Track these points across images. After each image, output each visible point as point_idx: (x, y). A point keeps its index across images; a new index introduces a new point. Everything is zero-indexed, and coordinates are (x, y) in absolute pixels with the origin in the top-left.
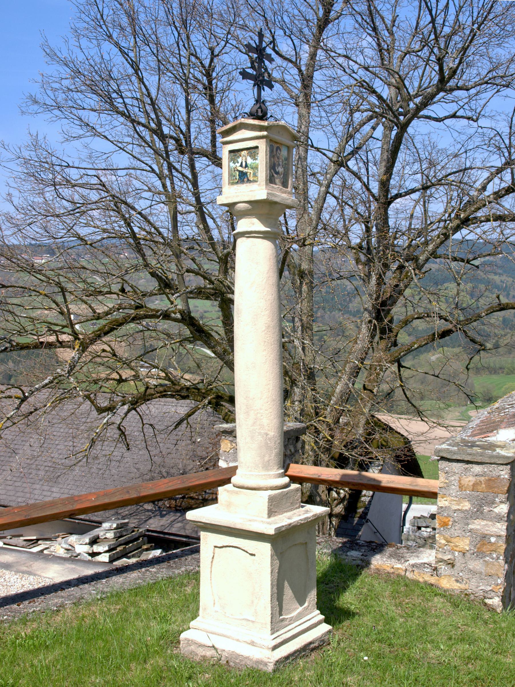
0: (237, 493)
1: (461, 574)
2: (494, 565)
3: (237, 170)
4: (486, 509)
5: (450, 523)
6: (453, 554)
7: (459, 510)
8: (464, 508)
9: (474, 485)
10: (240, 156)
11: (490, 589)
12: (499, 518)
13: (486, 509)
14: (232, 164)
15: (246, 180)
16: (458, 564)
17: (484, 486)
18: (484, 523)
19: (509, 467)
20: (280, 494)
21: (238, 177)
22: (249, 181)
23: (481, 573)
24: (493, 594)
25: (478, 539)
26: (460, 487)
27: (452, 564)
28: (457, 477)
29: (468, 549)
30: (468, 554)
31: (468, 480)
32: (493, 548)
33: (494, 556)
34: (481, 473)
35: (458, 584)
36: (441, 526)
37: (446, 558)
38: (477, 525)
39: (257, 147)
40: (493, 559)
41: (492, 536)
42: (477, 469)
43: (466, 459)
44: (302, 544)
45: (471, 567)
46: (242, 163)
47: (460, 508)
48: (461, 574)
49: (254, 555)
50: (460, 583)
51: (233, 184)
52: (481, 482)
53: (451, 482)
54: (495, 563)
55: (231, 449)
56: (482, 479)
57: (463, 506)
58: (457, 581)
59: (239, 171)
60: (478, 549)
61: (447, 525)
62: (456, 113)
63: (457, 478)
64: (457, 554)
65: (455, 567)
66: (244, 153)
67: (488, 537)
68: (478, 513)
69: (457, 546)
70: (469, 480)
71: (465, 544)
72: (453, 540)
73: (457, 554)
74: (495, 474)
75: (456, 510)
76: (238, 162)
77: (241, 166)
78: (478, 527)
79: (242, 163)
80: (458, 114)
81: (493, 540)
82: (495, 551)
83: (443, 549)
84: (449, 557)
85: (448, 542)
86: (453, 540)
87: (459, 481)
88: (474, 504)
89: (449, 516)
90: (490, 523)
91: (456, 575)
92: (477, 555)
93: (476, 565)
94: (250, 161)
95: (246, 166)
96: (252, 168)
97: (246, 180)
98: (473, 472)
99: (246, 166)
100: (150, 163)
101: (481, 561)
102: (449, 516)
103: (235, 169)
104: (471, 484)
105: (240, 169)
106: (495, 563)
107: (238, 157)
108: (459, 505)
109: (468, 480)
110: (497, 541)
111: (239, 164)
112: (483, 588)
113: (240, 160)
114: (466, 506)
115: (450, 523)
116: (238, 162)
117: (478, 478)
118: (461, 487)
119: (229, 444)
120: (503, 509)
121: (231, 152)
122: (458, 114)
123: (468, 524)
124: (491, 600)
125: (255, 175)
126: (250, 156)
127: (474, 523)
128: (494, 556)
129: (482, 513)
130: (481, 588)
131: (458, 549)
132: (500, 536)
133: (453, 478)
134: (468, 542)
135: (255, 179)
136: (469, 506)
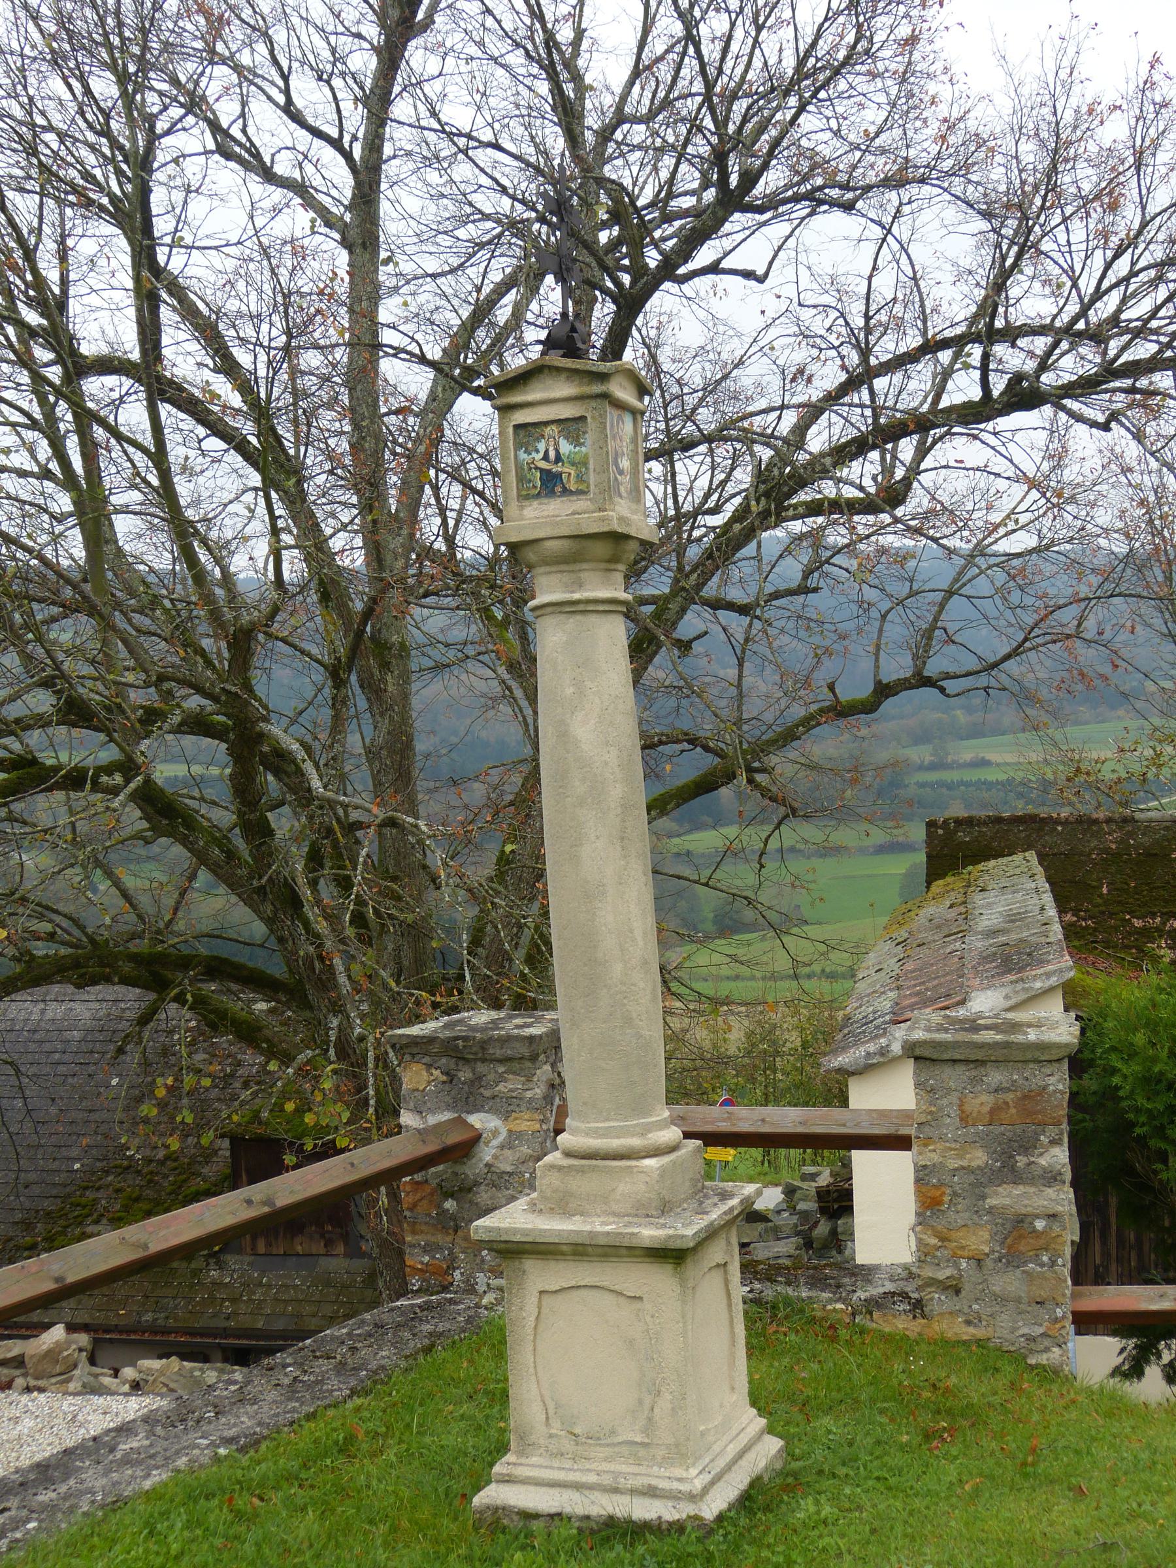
0: (581, 1170)
1: (976, 1307)
2: (1046, 1279)
3: (536, 468)
4: (1021, 1161)
5: (946, 1199)
6: (957, 1266)
7: (963, 1168)
8: (974, 1164)
9: (992, 1112)
10: (543, 436)
11: (1042, 1330)
12: (1051, 1178)
13: (1021, 1161)
14: (522, 455)
15: (559, 489)
16: (967, 1288)
17: (1013, 1111)
18: (1019, 1190)
19: (1065, 1065)
20: (674, 1162)
21: (539, 484)
22: (566, 492)
23: (1019, 1300)
24: (1047, 1342)
25: (1008, 1226)
26: (961, 1119)
27: (954, 1288)
28: (954, 1098)
29: (987, 1250)
30: (989, 1263)
31: (978, 1101)
32: (1042, 1242)
33: (1045, 1259)
34: (1005, 1085)
35: (971, 1330)
36: (927, 1208)
37: (941, 1275)
38: (1005, 1197)
39: (582, 418)
40: (1042, 1265)
41: (1037, 1216)
42: (995, 1077)
43: (973, 1057)
44: (718, 1265)
45: (996, 1289)
46: (546, 452)
47: (964, 1163)
48: (976, 1307)
49: (640, 1298)
50: (975, 1326)
51: (527, 497)
52: (1006, 1103)
53: (941, 1109)
54: (1049, 1275)
55: (429, 1082)
56: (1009, 1097)
57: (970, 1160)
58: (968, 1323)
59: (542, 470)
60: (1010, 1247)
61: (939, 1203)
62: (719, 261)
63: (956, 1101)
64: (964, 1264)
65: (963, 1293)
66: (548, 430)
67: (1029, 1219)
68: (1007, 1171)
69: (963, 1248)
70: (981, 1102)
71: (980, 1240)
72: (954, 1235)
73: (964, 1264)
74: (1037, 1081)
75: (956, 1169)
76: (537, 451)
77: (546, 457)
78: (1007, 1201)
79: (546, 452)
80: (724, 264)
81: (1040, 1225)
82: (1046, 1250)
83: (934, 1257)
84: (948, 1272)
85: (942, 1239)
86: (954, 1235)
87: (960, 1106)
88: (995, 1152)
89: (941, 1184)
90: (1032, 1190)
91: (966, 1310)
92: (1008, 1262)
93: (1008, 1282)
94: (565, 447)
95: (558, 459)
96: (573, 464)
97: (559, 489)
98: (989, 1084)
99: (558, 459)
100: (25, 405)
101: (1018, 1271)
102: (941, 1184)
103: (532, 466)
104: (986, 1109)
105: (543, 465)
106: (1049, 1275)
107: (538, 440)
108: (962, 1158)
109: (978, 1101)
110: (1048, 1228)
111: (541, 455)
112: (1025, 1331)
113: (541, 446)
114: (979, 1157)
115: (946, 1199)
116: (537, 451)
117: (1001, 1096)
118: (965, 1119)
119: (424, 1073)
120: (1059, 1156)
121: (517, 427)
122: (724, 264)
123: (983, 1197)
124: (1045, 1356)
125: (580, 479)
126: (566, 438)
127: (996, 1193)
128: (1045, 1259)
129: (1013, 1169)
130: (1021, 1332)
131: (966, 1254)
132: (1054, 1216)
133: (945, 1101)
134: (987, 1236)
135: (582, 487)
136: (985, 1158)
